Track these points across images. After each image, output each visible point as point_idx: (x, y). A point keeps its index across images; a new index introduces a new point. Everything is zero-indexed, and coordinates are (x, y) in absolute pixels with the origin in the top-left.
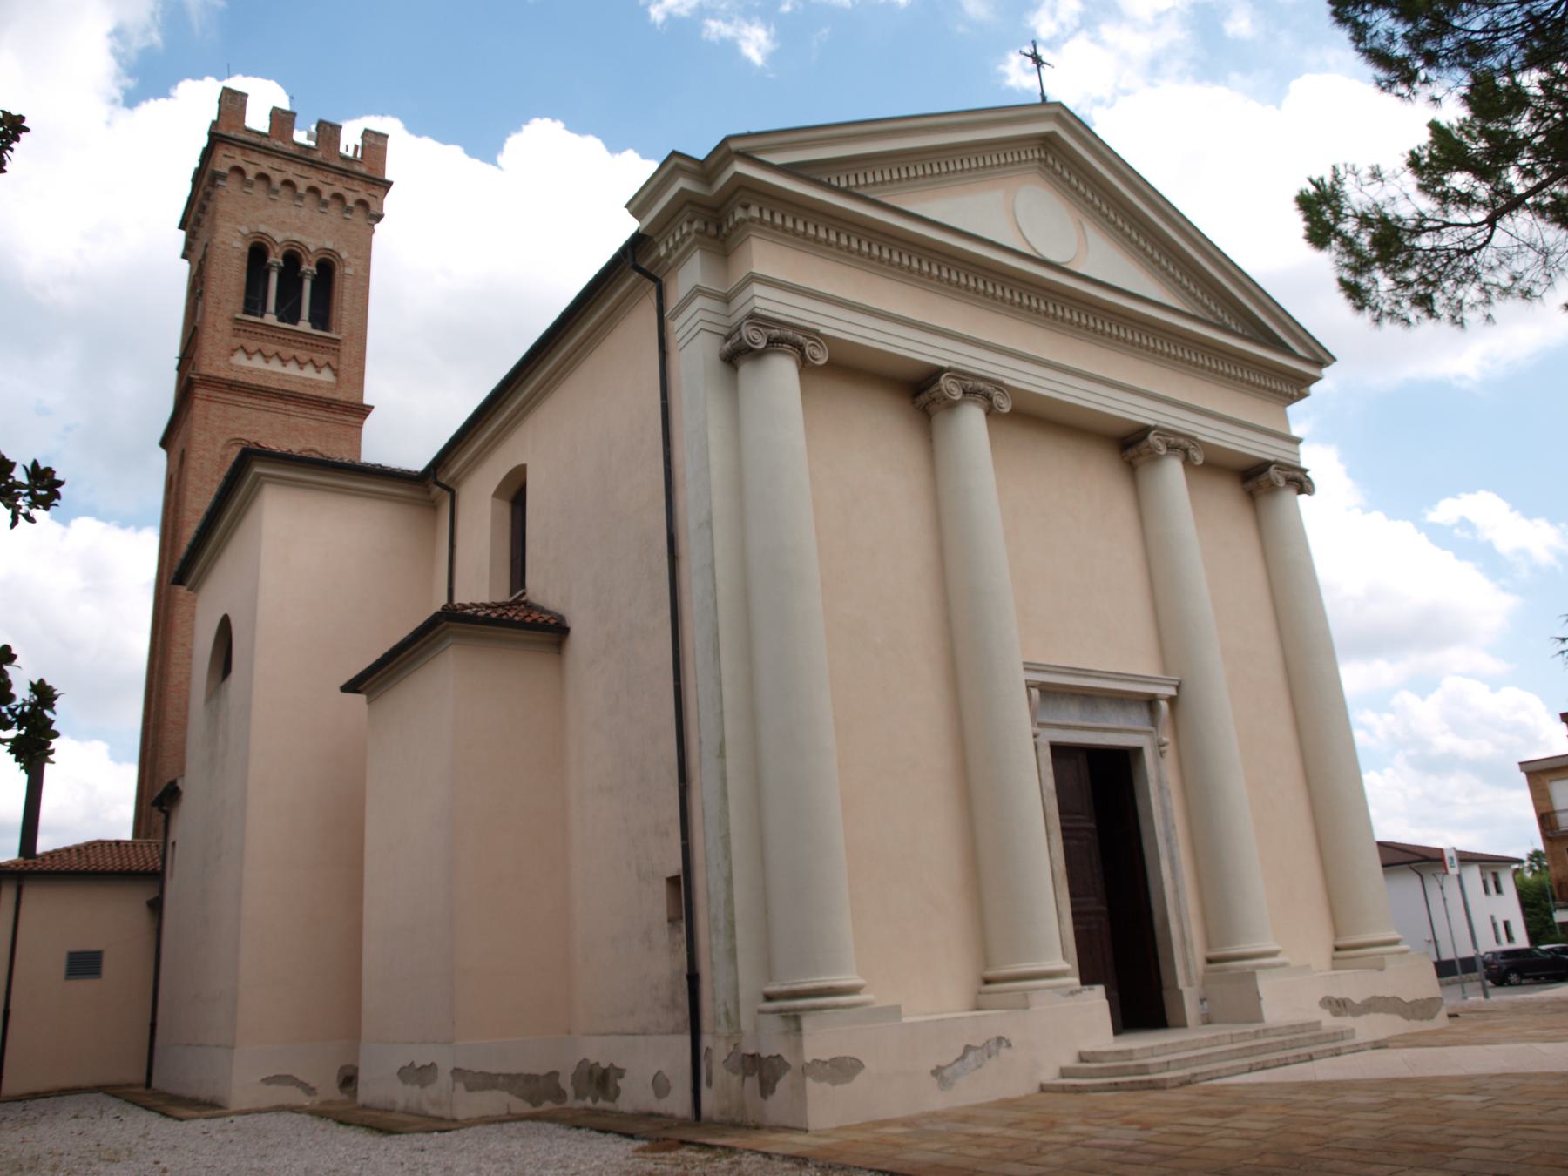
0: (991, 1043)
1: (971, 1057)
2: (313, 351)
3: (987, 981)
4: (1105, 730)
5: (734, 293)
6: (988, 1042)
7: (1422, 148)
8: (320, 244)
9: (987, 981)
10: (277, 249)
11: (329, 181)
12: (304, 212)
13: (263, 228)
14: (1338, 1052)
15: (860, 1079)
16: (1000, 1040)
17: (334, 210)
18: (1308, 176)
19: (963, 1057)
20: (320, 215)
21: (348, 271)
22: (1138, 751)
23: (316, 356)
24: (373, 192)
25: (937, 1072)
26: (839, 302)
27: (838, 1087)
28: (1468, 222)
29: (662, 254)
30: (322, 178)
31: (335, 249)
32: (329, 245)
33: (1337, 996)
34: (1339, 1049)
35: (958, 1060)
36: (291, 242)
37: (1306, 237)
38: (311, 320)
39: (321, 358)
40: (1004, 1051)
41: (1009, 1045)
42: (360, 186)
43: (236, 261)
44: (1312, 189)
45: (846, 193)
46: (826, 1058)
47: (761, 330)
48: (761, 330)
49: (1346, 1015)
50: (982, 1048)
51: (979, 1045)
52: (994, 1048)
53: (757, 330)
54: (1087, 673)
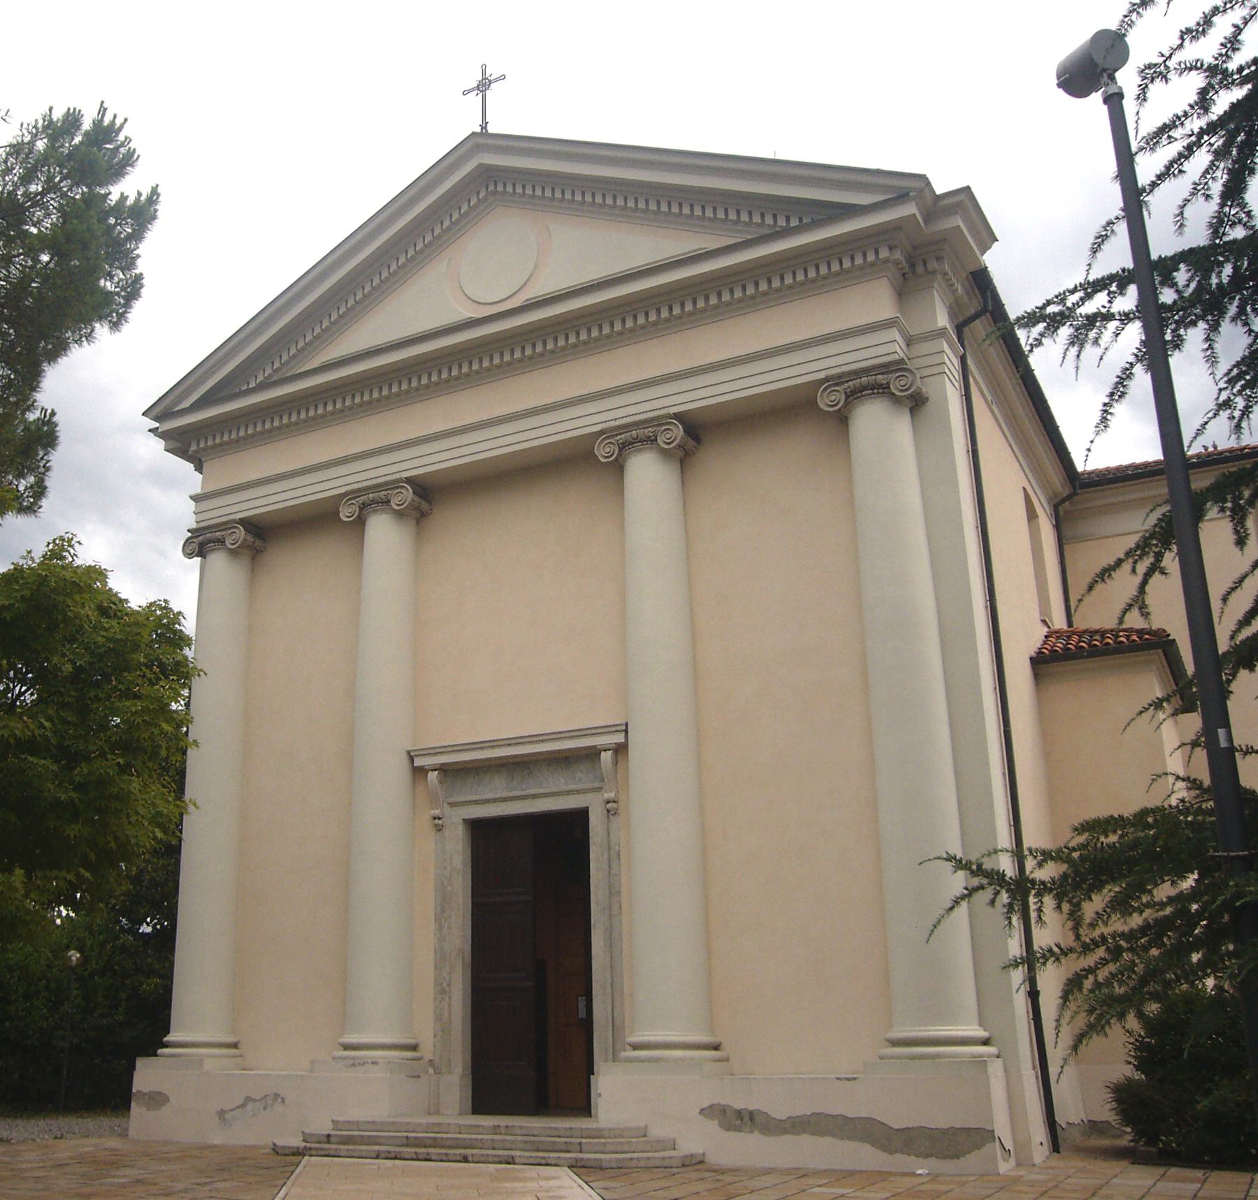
0: (268, 1098)
1: (250, 1107)
3: (235, 1046)
4: (535, 796)
5: (917, 339)
6: (266, 1096)
9: (235, 1046)
14: (511, 1160)
15: (165, 1110)
16: (277, 1096)
19: (243, 1106)
22: (581, 816)
25: (221, 1113)
26: (505, 419)
27: (982, 1150)
33: (739, 1105)
34: (513, 1157)
35: (238, 1107)
37: (140, 296)
40: (278, 1106)
41: (283, 1101)
45: (261, 387)
46: (146, 1091)
47: (837, 388)
48: (837, 388)
49: (752, 1132)
50: (259, 1101)
51: (258, 1098)
52: (270, 1102)
53: (834, 391)
54: (493, 744)
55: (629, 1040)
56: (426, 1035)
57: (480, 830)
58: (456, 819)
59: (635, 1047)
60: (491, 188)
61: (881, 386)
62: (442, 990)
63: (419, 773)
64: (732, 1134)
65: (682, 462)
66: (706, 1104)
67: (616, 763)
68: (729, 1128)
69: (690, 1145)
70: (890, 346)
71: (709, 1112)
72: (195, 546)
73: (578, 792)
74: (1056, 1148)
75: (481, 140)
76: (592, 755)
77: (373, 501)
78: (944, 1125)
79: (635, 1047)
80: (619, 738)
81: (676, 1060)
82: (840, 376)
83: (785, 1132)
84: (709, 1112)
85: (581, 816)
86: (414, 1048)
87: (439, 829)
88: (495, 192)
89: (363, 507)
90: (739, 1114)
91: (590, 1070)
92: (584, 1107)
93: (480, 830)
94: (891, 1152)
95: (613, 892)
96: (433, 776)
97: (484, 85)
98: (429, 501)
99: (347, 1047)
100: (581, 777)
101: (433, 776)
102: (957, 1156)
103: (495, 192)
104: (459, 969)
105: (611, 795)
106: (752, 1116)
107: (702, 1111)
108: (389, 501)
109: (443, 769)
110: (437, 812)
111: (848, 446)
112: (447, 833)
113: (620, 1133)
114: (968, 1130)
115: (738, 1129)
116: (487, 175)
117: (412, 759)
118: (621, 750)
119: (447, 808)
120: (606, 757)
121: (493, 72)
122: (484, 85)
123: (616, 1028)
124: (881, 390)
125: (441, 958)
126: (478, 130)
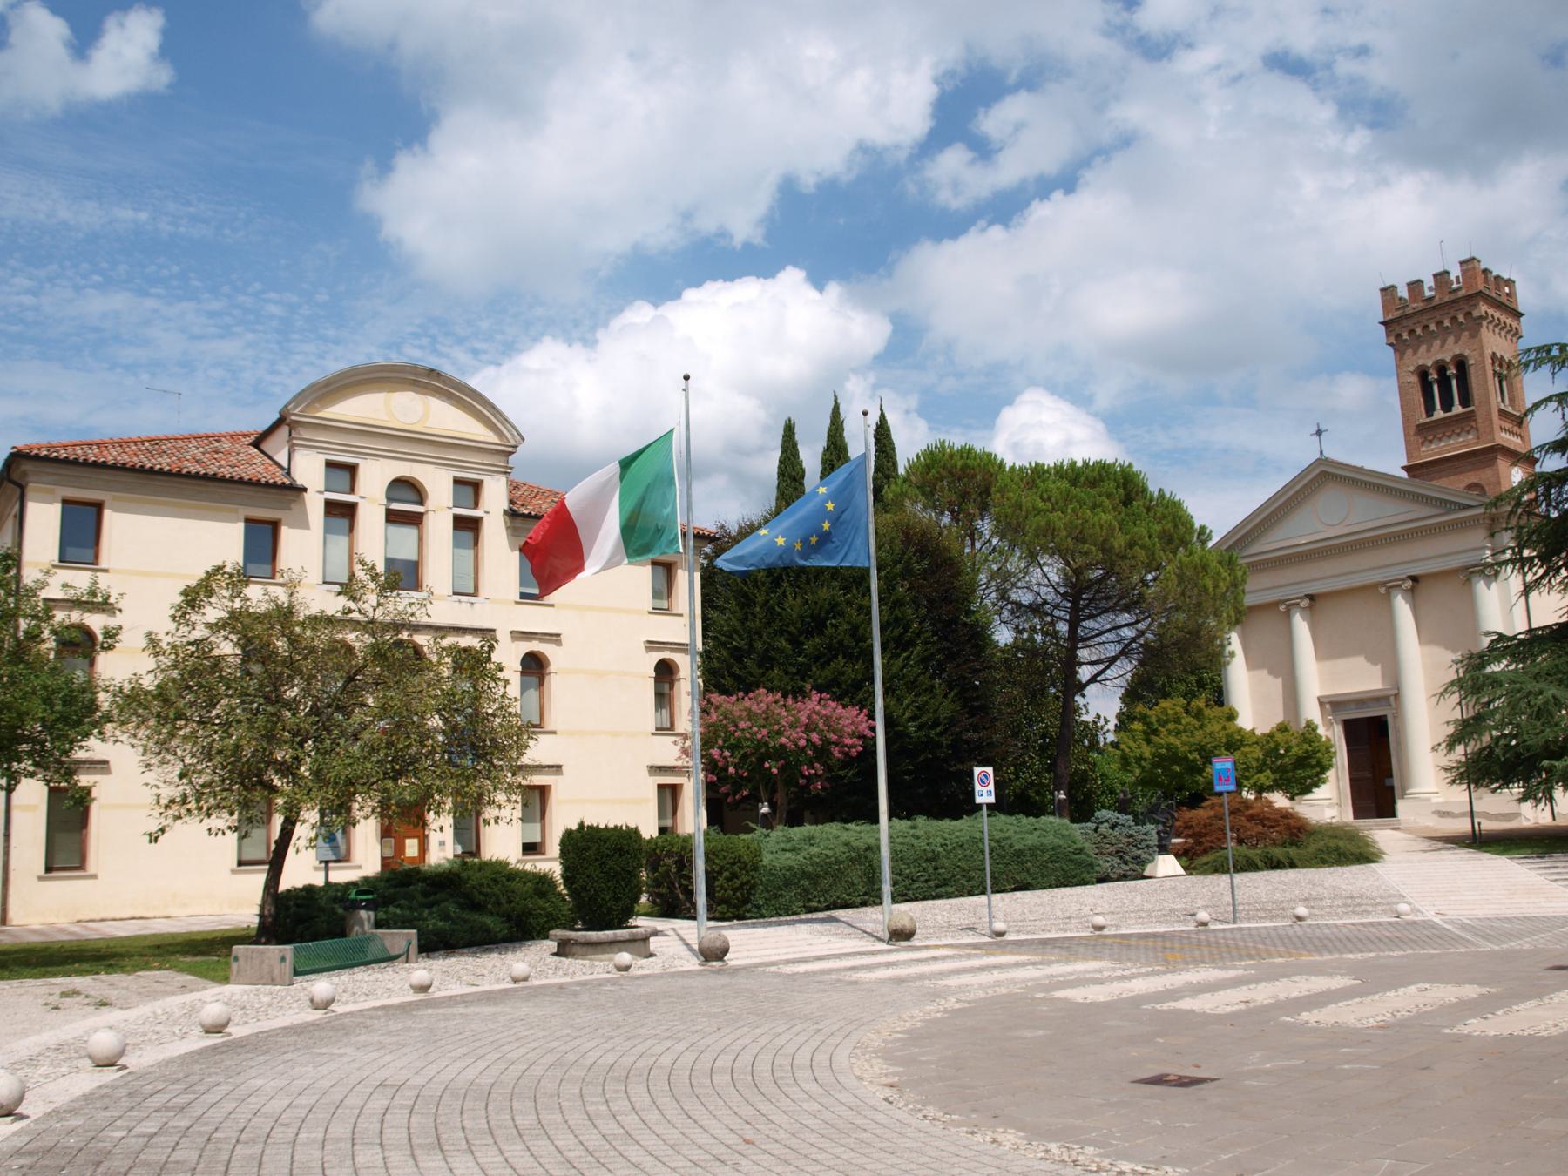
10: (1431, 371)
22: (1385, 716)
36: (1436, 362)
38: (1461, 404)
68: (1441, 817)
75: (1322, 461)
85: (1385, 716)
90: (1444, 813)
97: (1319, 433)
120: (1392, 698)
121: (1323, 427)
122: (1319, 433)
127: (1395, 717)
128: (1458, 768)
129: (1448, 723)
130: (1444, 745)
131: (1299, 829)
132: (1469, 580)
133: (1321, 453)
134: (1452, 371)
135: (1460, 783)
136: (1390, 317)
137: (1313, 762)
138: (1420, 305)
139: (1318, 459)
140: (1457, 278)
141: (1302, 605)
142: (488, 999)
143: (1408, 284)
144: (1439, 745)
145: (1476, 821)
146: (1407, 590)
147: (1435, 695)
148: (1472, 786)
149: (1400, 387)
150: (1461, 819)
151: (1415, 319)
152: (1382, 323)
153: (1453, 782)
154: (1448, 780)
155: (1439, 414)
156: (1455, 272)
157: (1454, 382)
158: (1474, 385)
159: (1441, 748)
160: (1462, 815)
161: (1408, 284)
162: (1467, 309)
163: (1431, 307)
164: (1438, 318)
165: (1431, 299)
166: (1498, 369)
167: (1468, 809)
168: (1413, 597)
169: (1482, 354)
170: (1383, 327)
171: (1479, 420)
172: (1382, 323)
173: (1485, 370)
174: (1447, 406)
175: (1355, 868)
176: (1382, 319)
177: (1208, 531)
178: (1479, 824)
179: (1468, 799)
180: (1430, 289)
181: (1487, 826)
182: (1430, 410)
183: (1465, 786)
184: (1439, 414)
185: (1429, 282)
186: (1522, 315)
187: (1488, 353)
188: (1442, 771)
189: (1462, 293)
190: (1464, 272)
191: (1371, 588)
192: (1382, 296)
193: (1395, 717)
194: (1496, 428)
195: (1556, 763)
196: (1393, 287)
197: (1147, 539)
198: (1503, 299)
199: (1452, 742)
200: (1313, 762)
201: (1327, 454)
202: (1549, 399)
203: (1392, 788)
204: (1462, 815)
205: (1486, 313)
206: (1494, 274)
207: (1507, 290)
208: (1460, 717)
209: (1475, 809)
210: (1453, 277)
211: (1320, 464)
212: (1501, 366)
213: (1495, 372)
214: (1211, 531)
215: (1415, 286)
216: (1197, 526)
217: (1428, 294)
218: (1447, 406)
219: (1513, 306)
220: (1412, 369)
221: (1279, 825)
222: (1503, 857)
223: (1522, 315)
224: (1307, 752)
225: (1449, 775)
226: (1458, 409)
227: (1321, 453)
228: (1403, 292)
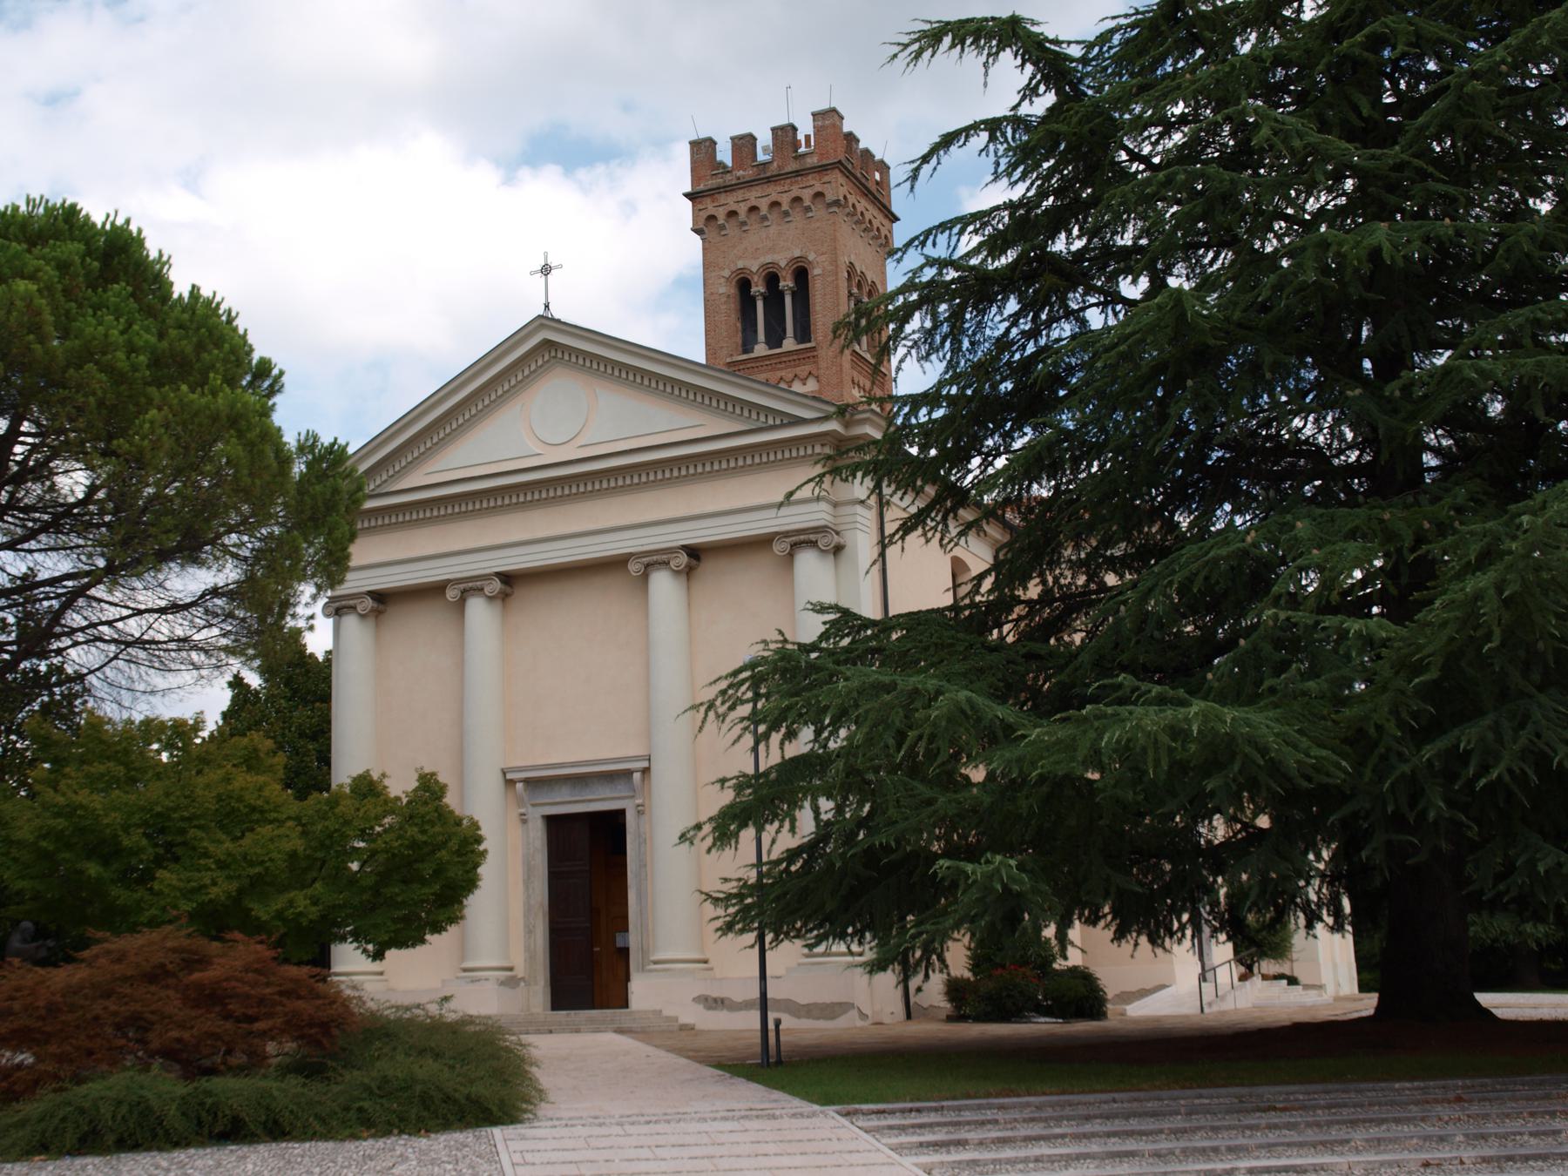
2: (795, 366)
7: (311, 622)
8: (789, 256)
10: (756, 278)
11: (786, 188)
12: (773, 230)
13: (740, 264)
17: (797, 217)
18: (197, 283)
20: (787, 225)
21: (817, 271)
22: (622, 812)
23: (798, 370)
24: (826, 179)
28: (36, 555)
29: (1051, 199)
30: (779, 189)
31: (803, 254)
32: (797, 253)
36: (765, 266)
38: (795, 337)
39: (803, 370)
42: (813, 178)
43: (723, 307)
44: (481, 848)
55: (652, 958)
56: (519, 961)
57: (555, 824)
58: (536, 816)
59: (656, 962)
60: (553, 354)
61: (811, 542)
62: (529, 931)
63: (510, 783)
64: (711, 1013)
65: (688, 574)
66: (696, 995)
67: (643, 780)
68: (709, 1008)
69: (685, 1019)
70: (818, 515)
71: (697, 1000)
72: (331, 610)
73: (619, 798)
74: (909, 1016)
75: (545, 321)
76: (628, 774)
77: (471, 589)
78: (828, 1001)
79: (656, 962)
80: (645, 764)
81: (681, 970)
82: (788, 532)
83: (741, 1009)
84: (697, 1000)
85: (622, 812)
86: (511, 969)
87: (524, 822)
88: (555, 357)
89: (464, 591)
90: (715, 1000)
91: (628, 979)
92: (625, 1005)
93: (555, 824)
94: (799, 1017)
95: (643, 865)
96: (519, 786)
97: (546, 270)
98: (511, 586)
99: (465, 970)
100: (620, 789)
101: (519, 786)
102: (833, 1018)
103: (555, 357)
104: (540, 915)
105: (639, 801)
106: (723, 1001)
107: (694, 999)
108: (482, 589)
109: (527, 781)
110: (523, 811)
111: (793, 580)
112: (530, 824)
113: (639, 1012)
114: (840, 1004)
115: (715, 1009)
116: (548, 344)
117: (504, 774)
118: (646, 771)
119: (530, 809)
120: (637, 776)
121: (553, 262)
122: (546, 270)
123: (644, 952)
124: (813, 544)
125: (528, 910)
126: (541, 312)
127: (640, 813)
128: (740, 896)
129: (723, 781)
130: (707, 828)
131: (325, 1027)
132: (791, 555)
133: (547, 306)
134: (787, 283)
135: (742, 931)
136: (702, 187)
137: (427, 869)
138: (746, 173)
139: (540, 317)
140: (807, 137)
141: (487, 590)
142: (425, 1101)
143: (732, 139)
144: (698, 827)
145: (771, 1016)
146: (677, 573)
147: (695, 707)
148: (769, 937)
149: (706, 300)
150: (743, 1013)
151: (739, 195)
152: (686, 195)
153: (728, 928)
154: (719, 923)
155: (761, 349)
156: (805, 128)
157: (788, 300)
158: (818, 308)
159: (701, 834)
160: (746, 1005)
161: (732, 139)
162: (818, 188)
163: (766, 177)
164: (774, 197)
165: (764, 164)
166: (855, 290)
167: (756, 994)
168: (688, 588)
169: (834, 262)
170: (689, 203)
171: (823, 364)
172: (686, 195)
173: (837, 287)
174: (775, 338)
175: (441, 1144)
176: (688, 189)
177: (275, 372)
178: (778, 1023)
179: (757, 973)
180: (765, 149)
181: (796, 1030)
182: (747, 346)
183: (751, 937)
184: (761, 349)
185: (764, 139)
186: (897, 219)
187: (844, 260)
188: (708, 905)
189: (813, 161)
190: (817, 130)
191: (613, 565)
192: (692, 149)
193: (640, 813)
194: (847, 380)
195: (969, 868)
196: (711, 143)
197: (121, 355)
198: (873, 188)
199: (726, 827)
200: (427, 869)
201: (557, 312)
202: (974, 128)
203: (624, 952)
204: (746, 1005)
205: (845, 197)
206: (862, 145)
207: (877, 176)
208: (750, 771)
209: (770, 995)
210: (801, 137)
211: (542, 326)
212: (859, 286)
213: (850, 294)
214: (282, 373)
215: (743, 144)
216: (256, 357)
217: (762, 157)
218: (775, 338)
219: (885, 201)
220: (727, 273)
221: (270, 1016)
222: (830, 1110)
223: (897, 219)
224: (414, 845)
225: (720, 912)
226: (789, 344)
227: (547, 306)
228: (724, 154)
